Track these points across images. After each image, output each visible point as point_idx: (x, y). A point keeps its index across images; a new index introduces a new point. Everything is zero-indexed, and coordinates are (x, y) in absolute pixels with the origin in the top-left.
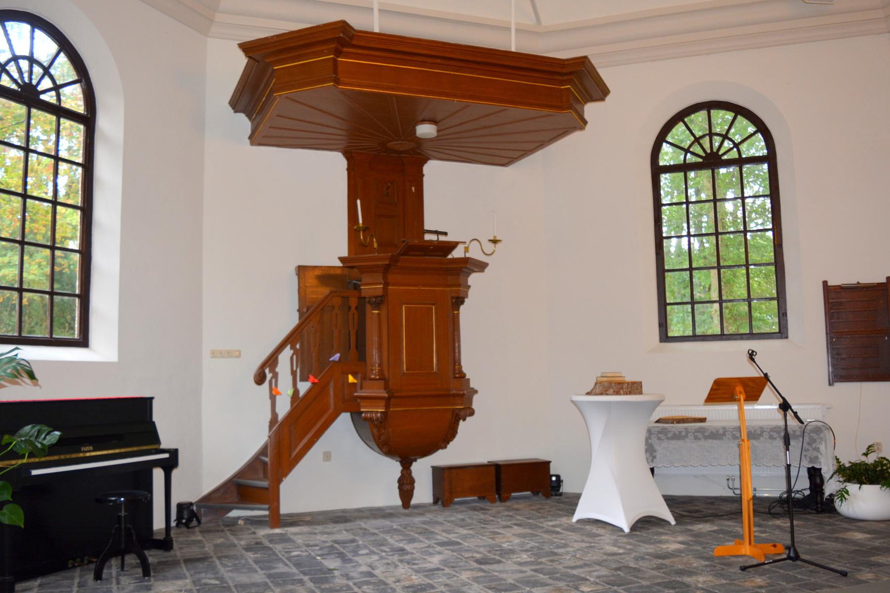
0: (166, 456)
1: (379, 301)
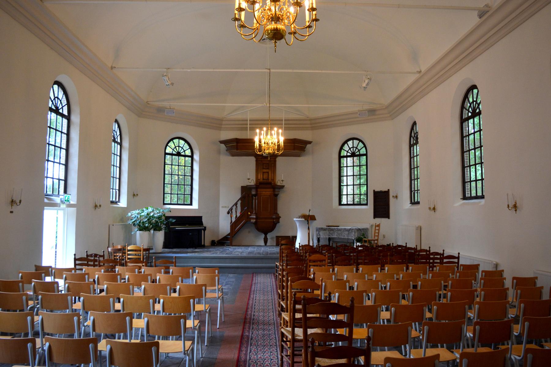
0: (204, 228)
1: (255, 195)
